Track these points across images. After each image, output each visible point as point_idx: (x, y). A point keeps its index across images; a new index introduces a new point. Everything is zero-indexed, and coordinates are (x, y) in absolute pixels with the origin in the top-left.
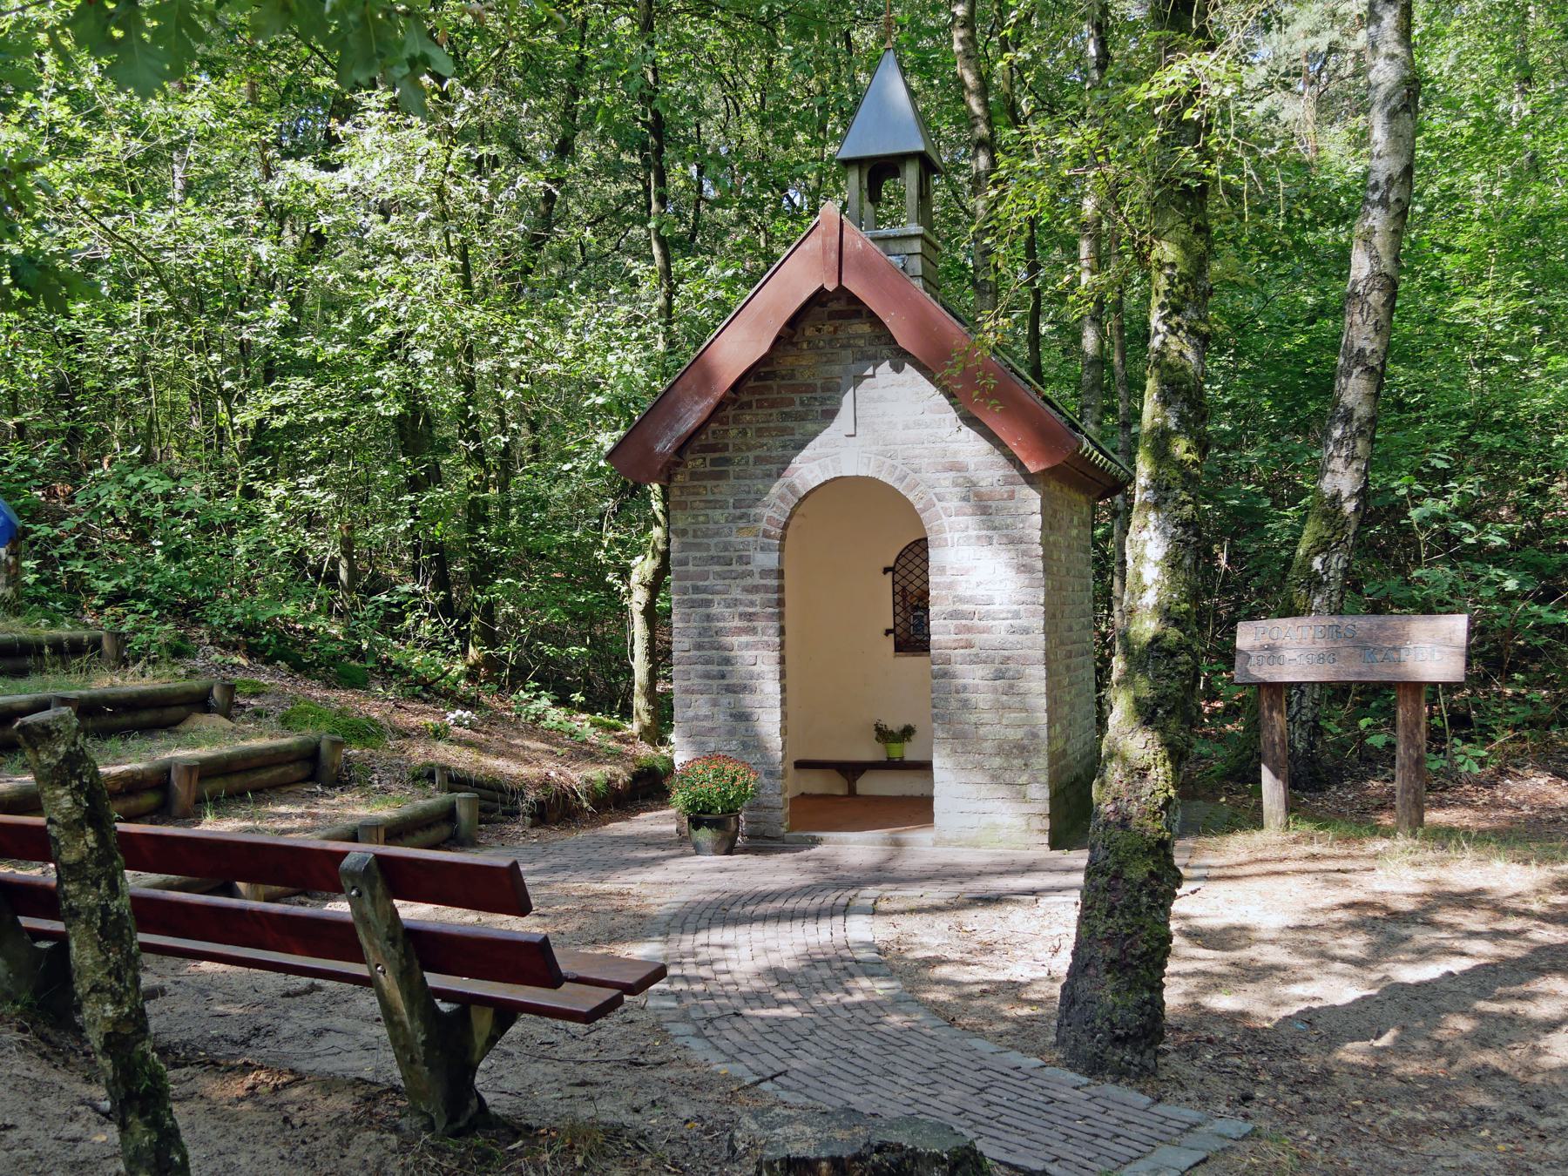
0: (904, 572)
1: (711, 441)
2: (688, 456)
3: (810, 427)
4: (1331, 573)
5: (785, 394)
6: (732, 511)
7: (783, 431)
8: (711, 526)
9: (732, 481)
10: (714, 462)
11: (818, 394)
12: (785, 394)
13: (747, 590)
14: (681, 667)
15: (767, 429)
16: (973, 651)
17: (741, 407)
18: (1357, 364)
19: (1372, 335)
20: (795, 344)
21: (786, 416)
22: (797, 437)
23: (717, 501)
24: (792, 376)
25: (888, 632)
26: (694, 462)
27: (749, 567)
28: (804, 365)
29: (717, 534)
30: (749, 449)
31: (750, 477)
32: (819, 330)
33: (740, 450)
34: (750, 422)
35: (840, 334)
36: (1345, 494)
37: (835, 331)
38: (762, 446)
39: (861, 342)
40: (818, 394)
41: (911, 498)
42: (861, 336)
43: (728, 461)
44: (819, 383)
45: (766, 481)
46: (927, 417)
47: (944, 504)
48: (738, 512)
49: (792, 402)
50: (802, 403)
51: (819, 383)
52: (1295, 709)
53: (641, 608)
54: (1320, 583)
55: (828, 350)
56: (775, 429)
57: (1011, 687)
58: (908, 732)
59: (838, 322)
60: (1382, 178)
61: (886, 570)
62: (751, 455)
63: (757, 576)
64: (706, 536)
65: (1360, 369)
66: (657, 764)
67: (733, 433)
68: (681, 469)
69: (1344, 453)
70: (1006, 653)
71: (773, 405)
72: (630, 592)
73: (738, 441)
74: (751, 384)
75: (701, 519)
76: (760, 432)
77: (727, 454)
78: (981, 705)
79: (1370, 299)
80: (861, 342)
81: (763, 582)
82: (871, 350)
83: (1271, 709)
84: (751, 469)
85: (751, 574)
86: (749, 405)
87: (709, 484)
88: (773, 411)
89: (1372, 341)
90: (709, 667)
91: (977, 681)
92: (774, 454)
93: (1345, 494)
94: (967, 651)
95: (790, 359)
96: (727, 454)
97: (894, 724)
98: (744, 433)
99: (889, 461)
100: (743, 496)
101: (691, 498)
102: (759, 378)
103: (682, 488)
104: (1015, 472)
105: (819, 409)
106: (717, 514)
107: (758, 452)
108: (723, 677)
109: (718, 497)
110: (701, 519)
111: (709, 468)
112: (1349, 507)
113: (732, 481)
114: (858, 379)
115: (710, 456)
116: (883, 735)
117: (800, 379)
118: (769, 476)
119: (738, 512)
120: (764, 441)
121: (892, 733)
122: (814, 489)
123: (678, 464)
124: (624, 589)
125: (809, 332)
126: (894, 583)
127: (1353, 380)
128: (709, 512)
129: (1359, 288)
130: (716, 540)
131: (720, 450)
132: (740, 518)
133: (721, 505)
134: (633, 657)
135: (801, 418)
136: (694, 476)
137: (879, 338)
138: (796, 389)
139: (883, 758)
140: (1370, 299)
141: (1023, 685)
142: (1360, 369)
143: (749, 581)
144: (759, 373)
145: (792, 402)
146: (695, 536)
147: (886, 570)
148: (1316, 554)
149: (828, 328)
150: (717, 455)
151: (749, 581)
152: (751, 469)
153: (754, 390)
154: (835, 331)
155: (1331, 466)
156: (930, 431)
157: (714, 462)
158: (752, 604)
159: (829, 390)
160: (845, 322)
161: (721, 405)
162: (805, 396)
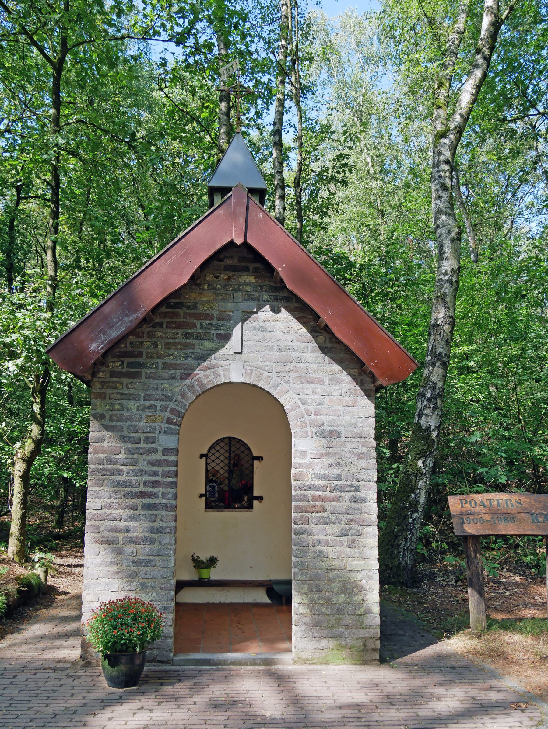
0: (213, 458)
1: (129, 349)
2: (110, 359)
3: (208, 345)
4: (427, 469)
5: (188, 320)
6: (142, 402)
7: (186, 346)
8: (125, 413)
9: (144, 380)
10: (130, 365)
11: (215, 321)
12: (188, 320)
13: (150, 463)
14: (92, 522)
15: (175, 344)
16: (325, 515)
17: (154, 326)
18: (438, 360)
19: (445, 346)
20: (198, 285)
21: (189, 336)
22: (197, 351)
23: (131, 394)
24: (195, 307)
25: (201, 496)
26: (114, 364)
27: (154, 446)
28: (205, 301)
29: (130, 419)
30: (159, 357)
31: (159, 378)
32: (217, 277)
33: (151, 357)
34: (161, 338)
35: (233, 282)
36: (433, 427)
37: (229, 278)
38: (169, 355)
39: (248, 289)
40: (215, 321)
41: (282, 401)
42: (248, 284)
43: (142, 365)
44: (215, 314)
45: (171, 381)
46: (296, 344)
47: (306, 407)
48: (147, 404)
49: (194, 326)
50: (202, 327)
51: (215, 314)
52: (409, 543)
53: (21, 474)
54: (422, 474)
55: (223, 291)
56: (180, 344)
57: (353, 541)
58: (212, 562)
59: (231, 273)
60: (449, 270)
61: (202, 456)
62: (160, 362)
63: (160, 453)
64: (120, 420)
65: (440, 363)
66: (33, 581)
67: (147, 344)
68: (103, 368)
69: (432, 406)
70: (350, 517)
71: (179, 326)
72: (13, 464)
73: (151, 351)
74: (163, 310)
75: (117, 407)
76: (168, 346)
77: (141, 360)
78: (331, 555)
79: (445, 328)
80: (248, 289)
81: (164, 457)
82: (256, 294)
83: (475, 552)
84: (160, 372)
85: (155, 451)
86: (161, 325)
87: (125, 381)
88: (180, 331)
89: (445, 349)
90: (117, 523)
91: (328, 537)
92: (178, 362)
93: (433, 427)
94: (321, 515)
95: (194, 295)
96: (141, 360)
97: (204, 557)
98: (156, 345)
99: (266, 373)
100: (152, 392)
101: (110, 391)
102: (169, 306)
103: (103, 383)
104: (357, 387)
105: (215, 332)
106: (130, 404)
107: (166, 360)
108: (128, 531)
109: (132, 391)
110: (117, 407)
111: (125, 369)
112: (435, 434)
113: (144, 380)
114: (246, 316)
115: (127, 360)
116: (198, 563)
117: (201, 310)
118: (174, 378)
119: (147, 404)
120: (171, 352)
121: (202, 562)
122: (232, 383)
123: (103, 364)
124: (9, 461)
125: (210, 277)
126: (207, 464)
127: (436, 368)
128: (125, 402)
129: (439, 322)
130: (128, 424)
131: (136, 356)
132: (149, 408)
133: (136, 398)
134: (11, 505)
135: (200, 337)
136: (113, 374)
137: (261, 287)
138: (197, 316)
139: (196, 578)
140: (445, 328)
141: (362, 540)
142: (440, 363)
143: (152, 457)
144: (173, 302)
145: (194, 326)
146: (111, 420)
147: (202, 456)
148: (420, 458)
149: (224, 276)
150: (133, 360)
151: (152, 457)
152: (160, 372)
153: (165, 315)
154: (229, 278)
155: (425, 412)
156: (297, 354)
157: (130, 365)
158: (155, 474)
159: (223, 319)
160: (237, 274)
161: (144, 320)
162: (204, 322)
